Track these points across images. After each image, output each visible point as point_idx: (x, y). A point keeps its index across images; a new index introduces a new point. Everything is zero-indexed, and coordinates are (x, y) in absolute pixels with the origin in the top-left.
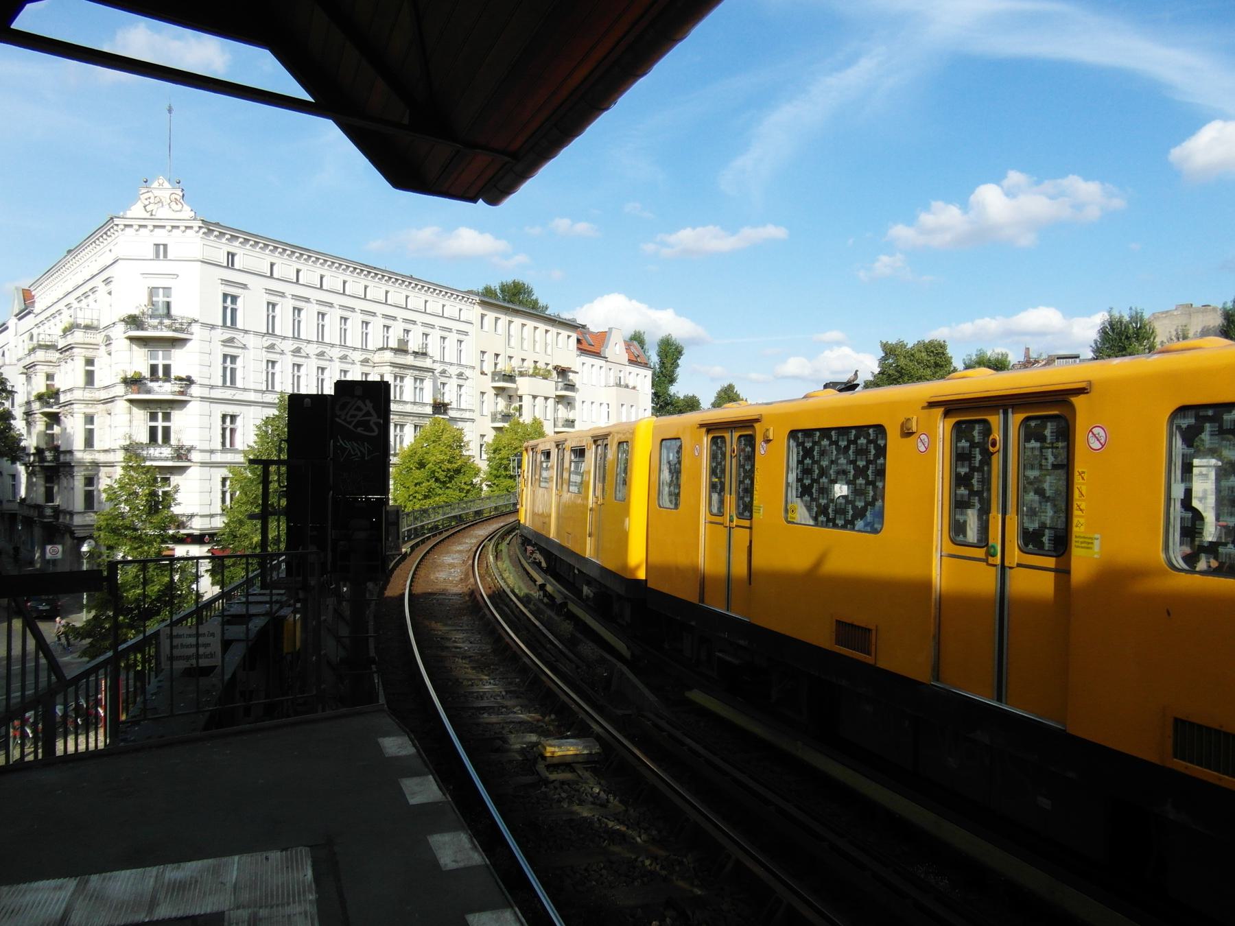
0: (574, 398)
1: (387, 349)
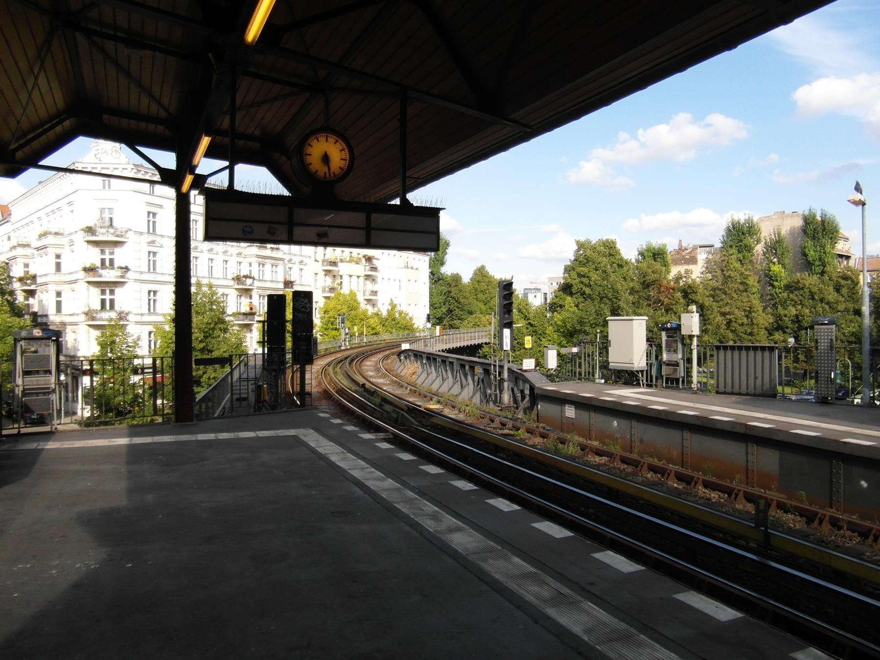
0: (377, 277)
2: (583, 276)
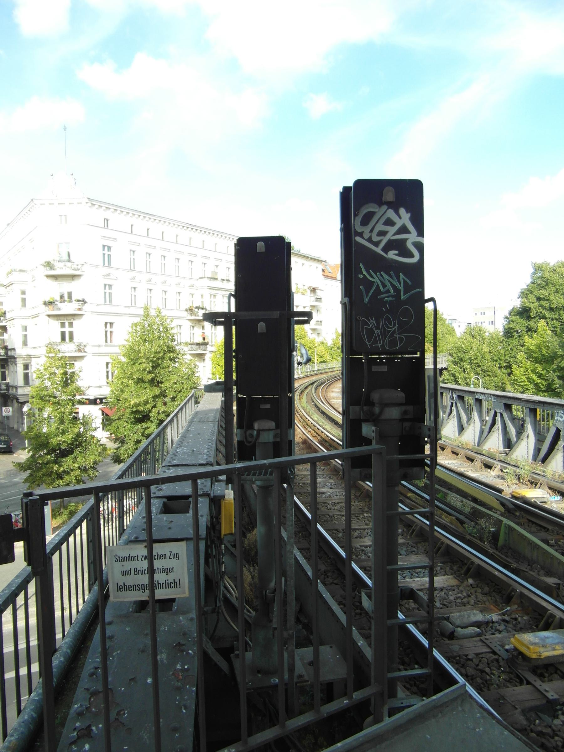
1: (204, 278)
2: (543, 299)
